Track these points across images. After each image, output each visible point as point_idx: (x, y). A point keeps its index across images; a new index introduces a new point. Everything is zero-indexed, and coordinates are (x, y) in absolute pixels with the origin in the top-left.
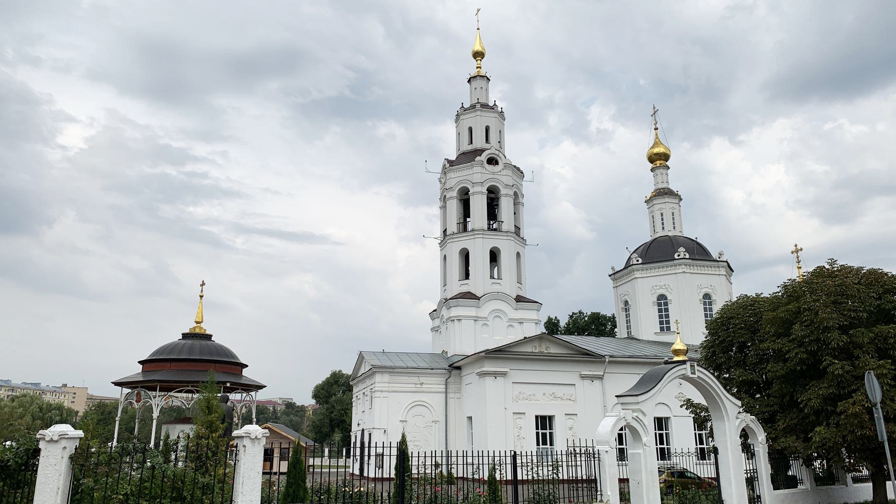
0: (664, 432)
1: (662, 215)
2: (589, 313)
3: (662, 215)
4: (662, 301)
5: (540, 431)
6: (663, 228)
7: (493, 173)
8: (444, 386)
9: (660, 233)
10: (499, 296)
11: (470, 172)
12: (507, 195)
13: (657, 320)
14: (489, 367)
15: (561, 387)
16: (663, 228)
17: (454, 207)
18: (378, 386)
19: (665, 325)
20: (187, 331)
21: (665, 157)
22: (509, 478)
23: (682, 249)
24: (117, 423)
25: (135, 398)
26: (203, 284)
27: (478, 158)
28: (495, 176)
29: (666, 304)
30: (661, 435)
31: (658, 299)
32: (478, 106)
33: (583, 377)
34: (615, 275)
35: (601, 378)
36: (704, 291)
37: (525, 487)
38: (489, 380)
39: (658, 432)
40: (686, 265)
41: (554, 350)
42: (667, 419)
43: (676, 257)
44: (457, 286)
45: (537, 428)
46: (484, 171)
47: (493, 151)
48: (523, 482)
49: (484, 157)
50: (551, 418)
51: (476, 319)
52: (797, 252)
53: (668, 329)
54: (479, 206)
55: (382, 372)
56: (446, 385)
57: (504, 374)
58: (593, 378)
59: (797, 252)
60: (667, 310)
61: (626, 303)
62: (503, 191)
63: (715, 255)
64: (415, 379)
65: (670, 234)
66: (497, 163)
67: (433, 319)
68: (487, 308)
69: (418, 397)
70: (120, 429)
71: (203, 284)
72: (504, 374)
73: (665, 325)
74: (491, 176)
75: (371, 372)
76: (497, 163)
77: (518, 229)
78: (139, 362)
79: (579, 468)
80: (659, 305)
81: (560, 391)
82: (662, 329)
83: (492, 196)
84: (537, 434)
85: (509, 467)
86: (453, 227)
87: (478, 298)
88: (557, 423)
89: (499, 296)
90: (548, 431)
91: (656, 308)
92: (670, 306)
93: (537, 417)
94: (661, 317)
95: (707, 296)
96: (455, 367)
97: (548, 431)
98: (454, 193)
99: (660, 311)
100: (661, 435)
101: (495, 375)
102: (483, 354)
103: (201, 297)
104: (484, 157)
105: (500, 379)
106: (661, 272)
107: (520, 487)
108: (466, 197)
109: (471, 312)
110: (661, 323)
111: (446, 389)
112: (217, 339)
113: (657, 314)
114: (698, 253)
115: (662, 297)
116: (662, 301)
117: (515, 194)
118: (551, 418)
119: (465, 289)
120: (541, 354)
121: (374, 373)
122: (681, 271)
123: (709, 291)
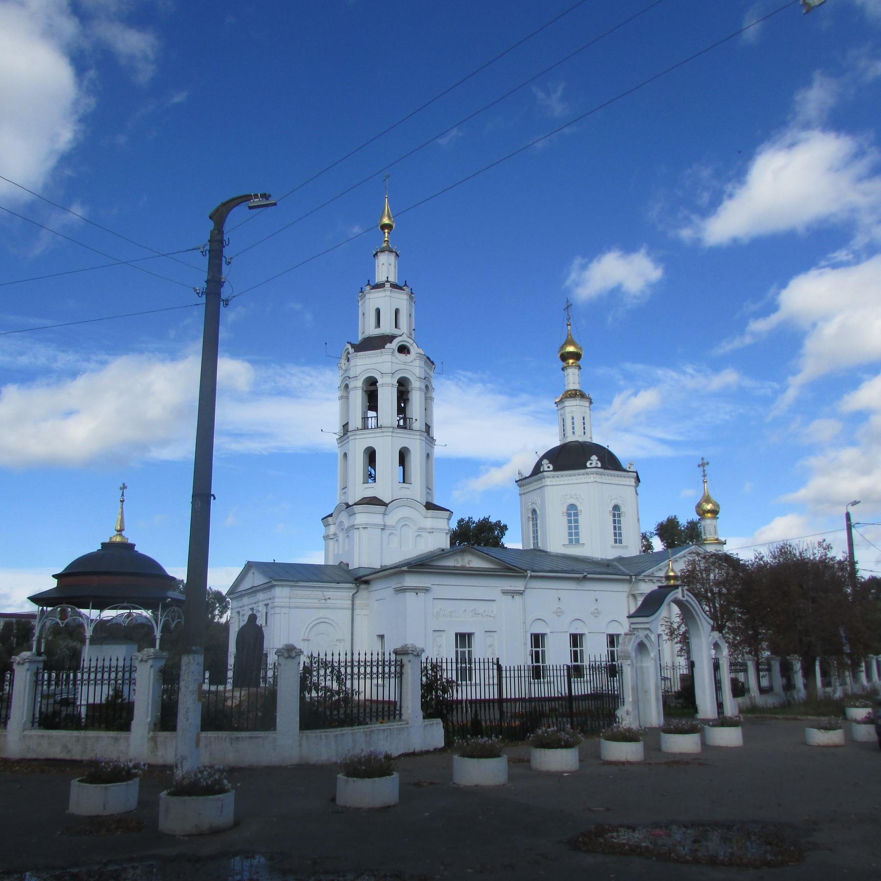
0: (540, 649)
1: (573, 419)
2: (476, 521)
3: (573, 419)
4: (572, 511)
5: (459, 650)
6: (574, 433)
8: (350, 602)
9: (570, 438)
10: (407, 502)
11: (380, 359)
13: (566, 531)
14: (410, 581)
15: (489, 603)
16: (574, 433)
17: (358, 398)
18: (278, 601)
19: (574, 535)
20: (107, 541)
22: (496, 697)
25: (58, 616)
26: (124, 487)
27: (388, 346)
28: (406, 367)
29: (576, 515)
30: (576, 652)
31: (568, 509)
32: (388, 285)
33: (505, 592)
34: (522, 482)
35: (521, 593)
37: (509, 704)
38: (410, 596)
39: (534, 649)
41: (476, 563)
42: (543, 635)
43: (588, 465)
44: (359, 490)
45: (457, 647)
46: (394, 360)
47: (404, 338)
48: (507, 700)
52: (703, 465)
53: (577, 541)
54: (387, 397)
55: (283, 586)
56: (353, 601)
57: (426, 590)
58: (513, 593)
59: (703, 465)
60: (576, 521)
61: (534, 511)
63: (625, 465)
64: (318, 593)
65: (581, 440)
66: (409, 352)
67: (327, 525)
68: (394, 517)
69: (322, 613)
71: (124, 487)
72: (426, 590)
73: (574, 535)
74: (403, 367)
75: (269, 585)
76: (409, 352)
77: (428, 428)
78: (54, 576)
80: (569, 515)
81: (481, 607)
82: (571, 541)
83: (402, 388)
84: (457, 652)
85: (496, 687)
86: (356, 422)
87: (386, 505)
88: (476, 642)
89: (407, 502)
90: (467, 650)
91: (566, 518)
92: (580, 518)
93: (456, 634)
94: (570, 528)
95: (616, 508)
96: (361, 580)
97: (467, 650)
98: (359, 383)
99: (570, 521)
100: (537, 653)
101: (416, 590)
102: (405, 568)
103: (122, 501)
105: (421, 595)
106: (573, 480)
107: (505, 704)
108: (373, 388)
109: (378, 519)
110: (570, 534)
111: (353, 604)
112: (140, 549)
113: (566, 524)
114: (610, 462)
115: (572, 507)
116: (572, 511)
118: (470, 635)
119: (369, 493)
120: (463, 568)
121: (273, 586)
122: (592, 480)
123: (619, 502)
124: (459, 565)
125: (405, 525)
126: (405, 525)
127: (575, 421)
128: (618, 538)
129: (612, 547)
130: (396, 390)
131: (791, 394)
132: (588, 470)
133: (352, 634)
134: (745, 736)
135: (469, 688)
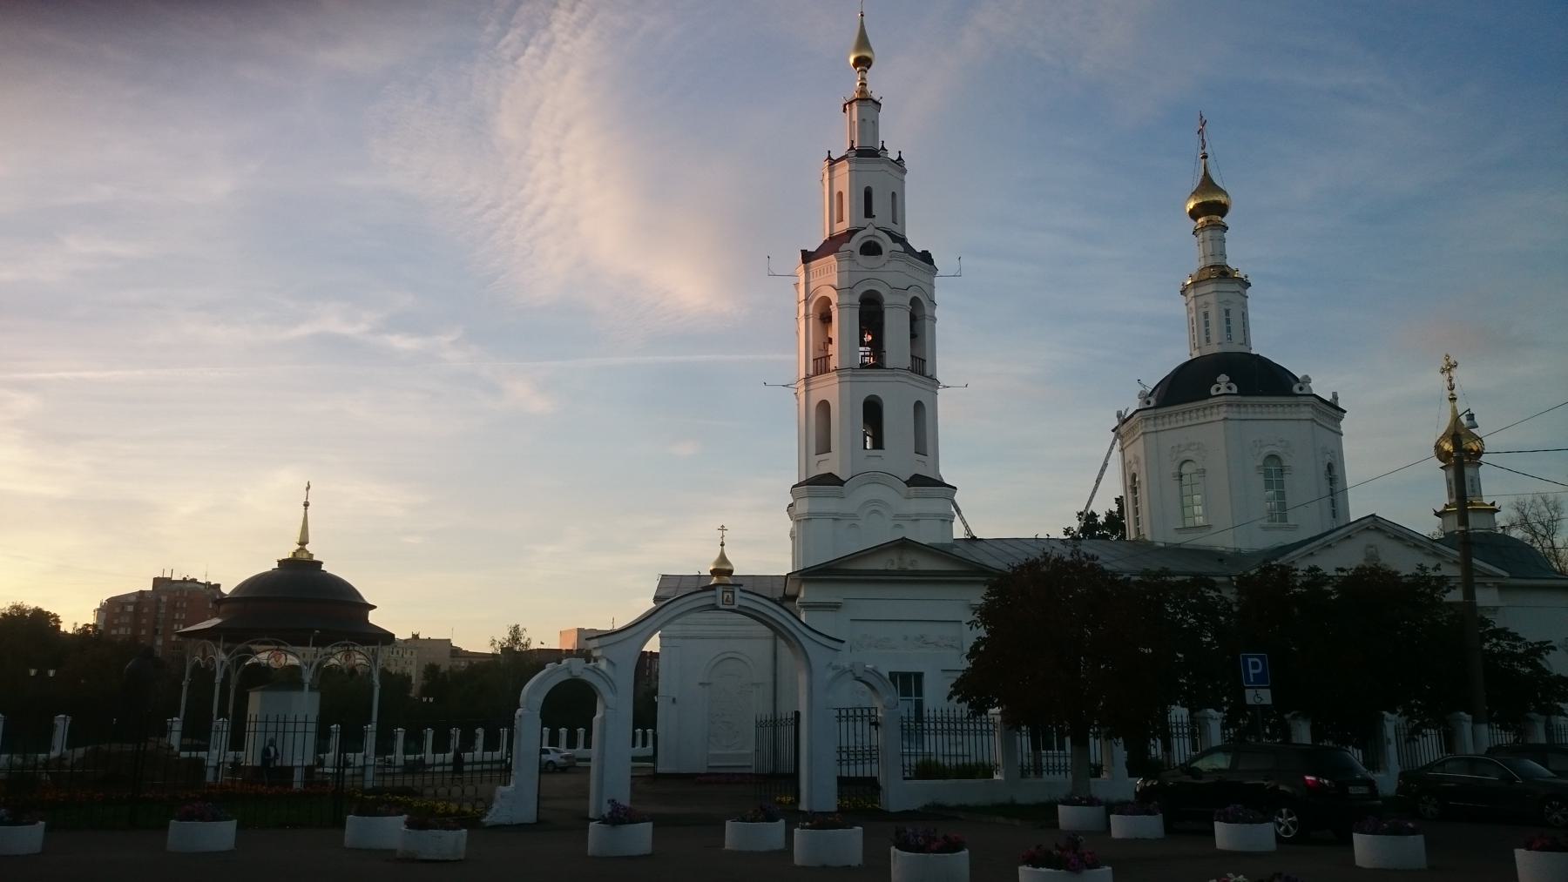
6: (1208, 340)
7: (872, 269)
9: (1214, 349)
10: (873, 477)
12: (893, 306)
16: (1208, 340)
21: (1222, 209)
23: (1223, 378)
24: (185, 690)
36: (1267, 450)
40: (1229, 405)
43: (1213, 392)
49: (856, 243)
50: (919, 676)
51: (836, 518)
57: (836, 607)
62: (888, 299)
70: (187, 701)
74: (868, 275)
79: (299, 736)
80: (1267, 473)
87: (841, 483)
89: (873, 477)
95: (878, 444)
104: (856, 243)
115: (1272, 457)
117: (915, 302)
118: (919, 676)
119: (823, 470)
120: (886, 572)
124: (895, 568)
125: (875, 511)
126: (875, 511)
127: (1231, 317)
128: (1280, 512)
129: (1265, 528)
130: (857, 312)
131: (304, 330)
132: (1210, 401)
133: (775, 675)
134: (1430, 845)
135: (299, 736)
